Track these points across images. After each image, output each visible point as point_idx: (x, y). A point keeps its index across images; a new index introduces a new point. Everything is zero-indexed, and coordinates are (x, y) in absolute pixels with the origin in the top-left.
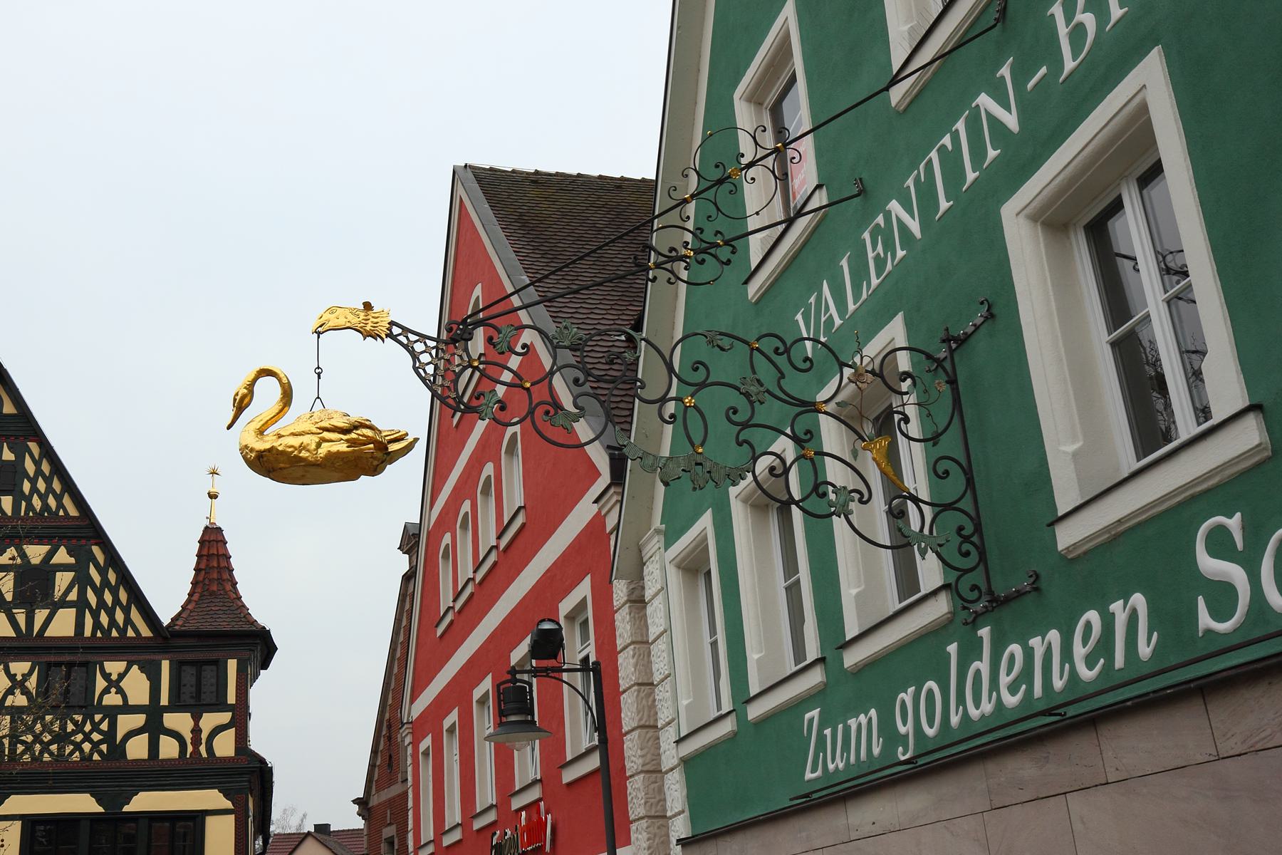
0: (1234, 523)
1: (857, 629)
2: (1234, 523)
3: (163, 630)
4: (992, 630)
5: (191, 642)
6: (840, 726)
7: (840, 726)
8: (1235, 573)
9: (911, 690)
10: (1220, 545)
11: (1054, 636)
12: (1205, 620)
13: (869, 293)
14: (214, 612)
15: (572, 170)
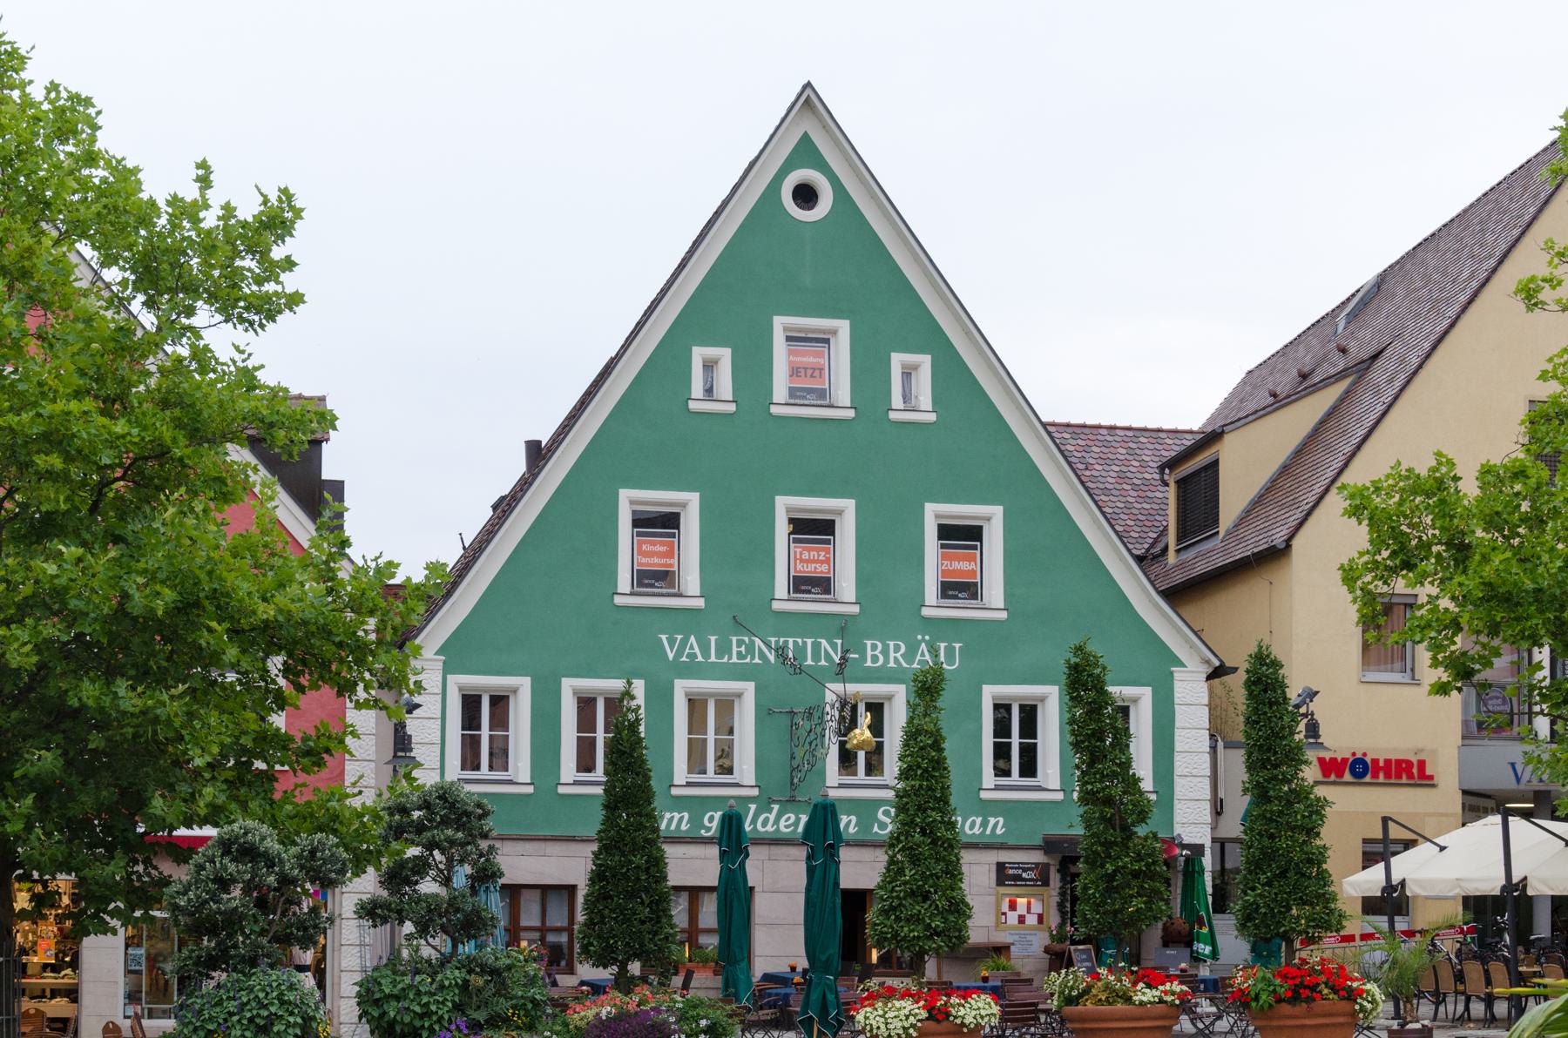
10: (886, 813)
12: (876, 829)
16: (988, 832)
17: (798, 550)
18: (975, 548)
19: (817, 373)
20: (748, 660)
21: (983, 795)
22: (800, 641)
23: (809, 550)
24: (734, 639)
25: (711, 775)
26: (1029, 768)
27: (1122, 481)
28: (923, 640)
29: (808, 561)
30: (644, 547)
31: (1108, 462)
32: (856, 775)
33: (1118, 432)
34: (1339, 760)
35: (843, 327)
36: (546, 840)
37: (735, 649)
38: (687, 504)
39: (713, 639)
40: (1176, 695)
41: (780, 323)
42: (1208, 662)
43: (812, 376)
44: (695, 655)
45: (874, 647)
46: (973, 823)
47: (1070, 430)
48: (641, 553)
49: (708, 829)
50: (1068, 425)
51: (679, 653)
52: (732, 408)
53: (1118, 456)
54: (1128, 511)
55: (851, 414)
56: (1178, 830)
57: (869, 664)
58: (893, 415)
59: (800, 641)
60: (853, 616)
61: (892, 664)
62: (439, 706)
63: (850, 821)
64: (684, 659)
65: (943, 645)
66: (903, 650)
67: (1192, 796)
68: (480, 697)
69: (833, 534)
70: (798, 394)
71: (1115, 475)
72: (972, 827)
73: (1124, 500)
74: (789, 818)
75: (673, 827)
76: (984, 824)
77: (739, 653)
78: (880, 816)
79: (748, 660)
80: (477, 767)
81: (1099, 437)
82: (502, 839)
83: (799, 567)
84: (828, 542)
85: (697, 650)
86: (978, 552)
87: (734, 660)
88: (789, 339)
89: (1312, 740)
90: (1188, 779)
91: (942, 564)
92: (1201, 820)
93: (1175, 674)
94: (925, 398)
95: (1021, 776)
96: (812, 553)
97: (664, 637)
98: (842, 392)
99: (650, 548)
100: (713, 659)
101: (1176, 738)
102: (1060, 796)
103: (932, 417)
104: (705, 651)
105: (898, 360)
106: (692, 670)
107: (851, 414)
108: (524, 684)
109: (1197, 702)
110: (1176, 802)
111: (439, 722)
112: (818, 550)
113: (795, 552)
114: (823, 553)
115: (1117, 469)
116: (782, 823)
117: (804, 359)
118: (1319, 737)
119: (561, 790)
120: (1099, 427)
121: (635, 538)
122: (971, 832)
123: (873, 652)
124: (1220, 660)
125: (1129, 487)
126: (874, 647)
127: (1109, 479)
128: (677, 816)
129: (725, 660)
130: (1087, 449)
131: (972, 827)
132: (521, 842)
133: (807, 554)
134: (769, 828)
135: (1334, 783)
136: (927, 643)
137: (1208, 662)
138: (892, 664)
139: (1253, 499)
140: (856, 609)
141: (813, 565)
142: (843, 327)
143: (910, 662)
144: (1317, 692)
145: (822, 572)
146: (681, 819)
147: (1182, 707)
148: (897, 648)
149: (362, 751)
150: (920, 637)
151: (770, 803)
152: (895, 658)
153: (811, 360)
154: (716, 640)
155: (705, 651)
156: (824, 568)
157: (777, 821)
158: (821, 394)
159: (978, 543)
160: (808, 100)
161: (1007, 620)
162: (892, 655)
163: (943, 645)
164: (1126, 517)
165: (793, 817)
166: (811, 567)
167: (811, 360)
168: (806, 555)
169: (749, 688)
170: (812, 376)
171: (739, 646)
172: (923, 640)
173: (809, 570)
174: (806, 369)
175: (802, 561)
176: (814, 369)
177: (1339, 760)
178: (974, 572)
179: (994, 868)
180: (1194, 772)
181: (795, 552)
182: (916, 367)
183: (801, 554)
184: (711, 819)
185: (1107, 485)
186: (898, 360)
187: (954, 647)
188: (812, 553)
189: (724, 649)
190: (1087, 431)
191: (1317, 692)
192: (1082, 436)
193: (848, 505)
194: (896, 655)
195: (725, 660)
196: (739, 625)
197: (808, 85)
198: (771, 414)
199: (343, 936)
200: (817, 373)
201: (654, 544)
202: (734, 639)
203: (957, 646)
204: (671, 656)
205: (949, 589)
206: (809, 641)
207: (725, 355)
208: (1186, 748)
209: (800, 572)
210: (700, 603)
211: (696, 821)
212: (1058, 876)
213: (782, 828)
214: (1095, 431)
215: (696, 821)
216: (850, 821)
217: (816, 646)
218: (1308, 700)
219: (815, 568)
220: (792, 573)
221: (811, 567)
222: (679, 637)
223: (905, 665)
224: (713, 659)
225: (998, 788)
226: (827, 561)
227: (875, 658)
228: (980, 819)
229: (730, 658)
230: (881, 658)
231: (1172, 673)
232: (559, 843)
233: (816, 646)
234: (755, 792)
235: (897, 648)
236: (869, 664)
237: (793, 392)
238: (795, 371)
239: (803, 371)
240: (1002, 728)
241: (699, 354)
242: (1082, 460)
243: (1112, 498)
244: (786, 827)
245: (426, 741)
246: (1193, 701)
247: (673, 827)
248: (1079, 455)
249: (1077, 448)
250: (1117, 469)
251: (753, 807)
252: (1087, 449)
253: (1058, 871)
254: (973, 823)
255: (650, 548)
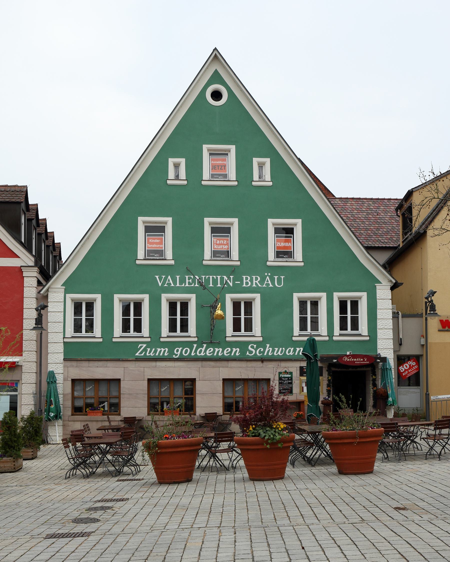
0: (255, 346)
1: (49, 309)
2: (255, 346)
3: (43, 267)
4: (206, 345)
5: (288, 261)
6: (154, 349)
7: (154, 349)
8: (254, 351)
9: (181, 348)
10: (252, 347)
11: (221, 349)
12: (248, 353)
13: (34, 253)
14: (5, 195)
15: (10, 183)
16: (296, 354)
17: (215, 240)
18: (291, 237)
19: (223, 168)
20: (193, 285)
21: (294, 339)
22: (215, 277)
23: (220, 240)
24: (187, 277)
25: (349, 331)
26: (355, 326)
27: (392, 219)
28: (268, 275)
29: (219, 244)
30: (150, 241)
31: (386, 212)
32: (176, 332)
33: (392, 201)
34: (444, 320)
35: (233, 148)
36: (107, 361)
37: (187, 281)
38: (167, 222)
39: (178, 277)
40: (377, 295)
41: (205, 147)
42: (391, 281)
43: (221, 169)
44: (170, 284)
45: (247, 279)
46: (290, 351)
47: (372, 201)
48: (149, 243)
49: (176, 355)
50: (372, 199)
51: (164, 283)
52: (185, 182)
53: (391, 210)
54: (393, 230)
55: (236, 183)
56: (379, 351)
57: (244, 285)
58: (254, 183)
59: (215, 277)
60: (237, 266)
61: (254, 285)
62: (63, 307)
63: (237, 350)
64: (166, 285)
65: (276, 277)
66: (259, 279)
67: (385, 337)
68: (81, 303)
69: (230, 233)
70: (215, 176)
71: (389, 217)
72: (289, 352)
73: (392, 226)
74: (210, 350)
75: (161, 354)
76: (295, 351)
77: (189, 283)
78: (250, 348)
79: (193, 285)
80: (176, 331)
81: (384, 203)
82: (89, 361)
83: (215, 247)
84: (228, 236)
85: (171, 282)
86: (292, 239)
87: (187, 285)
88: (211, 154)
89: (432, 312)
90: (383, 330)
91: (277, 244)
92: (389, 347)
93: (377, 287)
94: (267, 176)
95: (181, 332)
96: (221, 241)
97: (157, 277)
98: (232, 174)
99: (153, 241)
100: (178, 285)
101: (378, 313)
102: (327, 338)
103: (271, 184)
104: (175, 282)
105: (256, 161)
106: (169, 290)
107: (236, 183)
108: (98, 297)
109: (386, 298)
110: (378, 340)
111: (63, 313)
112: (223, 240)
113: (214, 241)
114: (226, 241)
115: (390, 214)
116: (208, 352)
117: (218, 162)
118: (435, 311)
119: (114, 340)
120: (384, 199)
121: (147, 237)
122: (289, 354)
123: (246, 281)
124: (395, 280)
125: (394, 221)
126: (247, 279)
127: (386, 219)
128: (163, 350)
129: (183, 285)
130: (378, 207)
131: (289, 352)
132: (97, 362)
133: (219, 241)
134: (202, 354)
135: (447, 331)
136: (269, 276)
137: (391, 281)
138: (254, 285)
139: (426, 218)
140: (238, 263)
141: (221, 246)
142: (233, 148)
143: (262, 284)
144: (435, 292)
145: (225, 249)
146: (165, 351)
147: (380, 300)
148: (256, 279)
149: (30, 326)
150: (266, 274)
151: (203, 344)
152: (256, 283)
153: (221, 162)
154: (179, 277)
155: (175, 282)
156: (226, 247)
157: (205, 351)
158: (225, 176)
159: (292, 235)
160: (216, 55)
161: (304, 266)
162: (254, 281)
163: (276, 277)
164: (392, 232)
165: (212, 349)
166: (221, 247)
167: (221, 162)
168: (218, 242)
169: (193, 297)
170: (221, 169)
171: (189, 279)
172: (268, 275)
173: (220, 248)
174: (218, 166)
175: (217, 244)
176: (222, 166)
177: (444, 320)
178: (290, 247)
179: (299, 369)
180: (386, 327)
181: (214, 241)
182: (264, 164)
183: (216, 241)
184: (177, 351)
185: (385, 221)
186: (256, 161)
187: (281, 278)
188: (221, 241)
189: (182, 281)
190: (379, 201)
191: (435, 292)
192: (377, 203)
193: (235, 221)
194: (256, 282)
195: (183, 285)
196: (189, 271)
197: (215, 49)
198: (202, 184)
199: (22, 401)
200: (223, 168)
201: (154, 239)
202: (187, 277)
203: (282, 277)
204: (160, 284)
205: (279, 254)
206: (219, 277)
207: (182, 161)
208: (382, 317)
209: (216, 249)
210: (173, 262)
211: (171, 352)
212: (327, 373)
213: (226, 354)
214: (382, 201)
215: (171, 352)
216: (237, 350)
217: (222, 279)
218: (431, 295)
219: (222, 247)
220: (212, 249)
221: (221, 247)
222: (164, 276)
223: (260, 286)
224: (178, 285)
225: (341, 335)
226: (227, 244)
227: (247, 283)
228: (293, 348)
229: (185, 284)
230: (250, 283)
231: (376, 286)
232: (113, 362)
233: (222, 279)
234: (196, 339)
235: (256, 279)
236: (244, 285)
237: (213, 176)
238: (214, 167)
239: (217, 167)
240: (303, 310)
241: (171, 161)
242: (376, 212)
243: (387, 225)
244: (209, 353)
245: (57, 321)
246: (385, 297)
247: (161, 354)
248: (375, 210)
249: (375, 207)
250: (390, 214)
251: (195, 345)
252: (378, 207)
253: (327, 371)
254: (290, 351)
255: (153, 241)
